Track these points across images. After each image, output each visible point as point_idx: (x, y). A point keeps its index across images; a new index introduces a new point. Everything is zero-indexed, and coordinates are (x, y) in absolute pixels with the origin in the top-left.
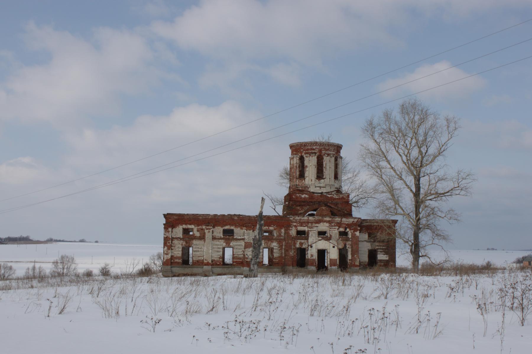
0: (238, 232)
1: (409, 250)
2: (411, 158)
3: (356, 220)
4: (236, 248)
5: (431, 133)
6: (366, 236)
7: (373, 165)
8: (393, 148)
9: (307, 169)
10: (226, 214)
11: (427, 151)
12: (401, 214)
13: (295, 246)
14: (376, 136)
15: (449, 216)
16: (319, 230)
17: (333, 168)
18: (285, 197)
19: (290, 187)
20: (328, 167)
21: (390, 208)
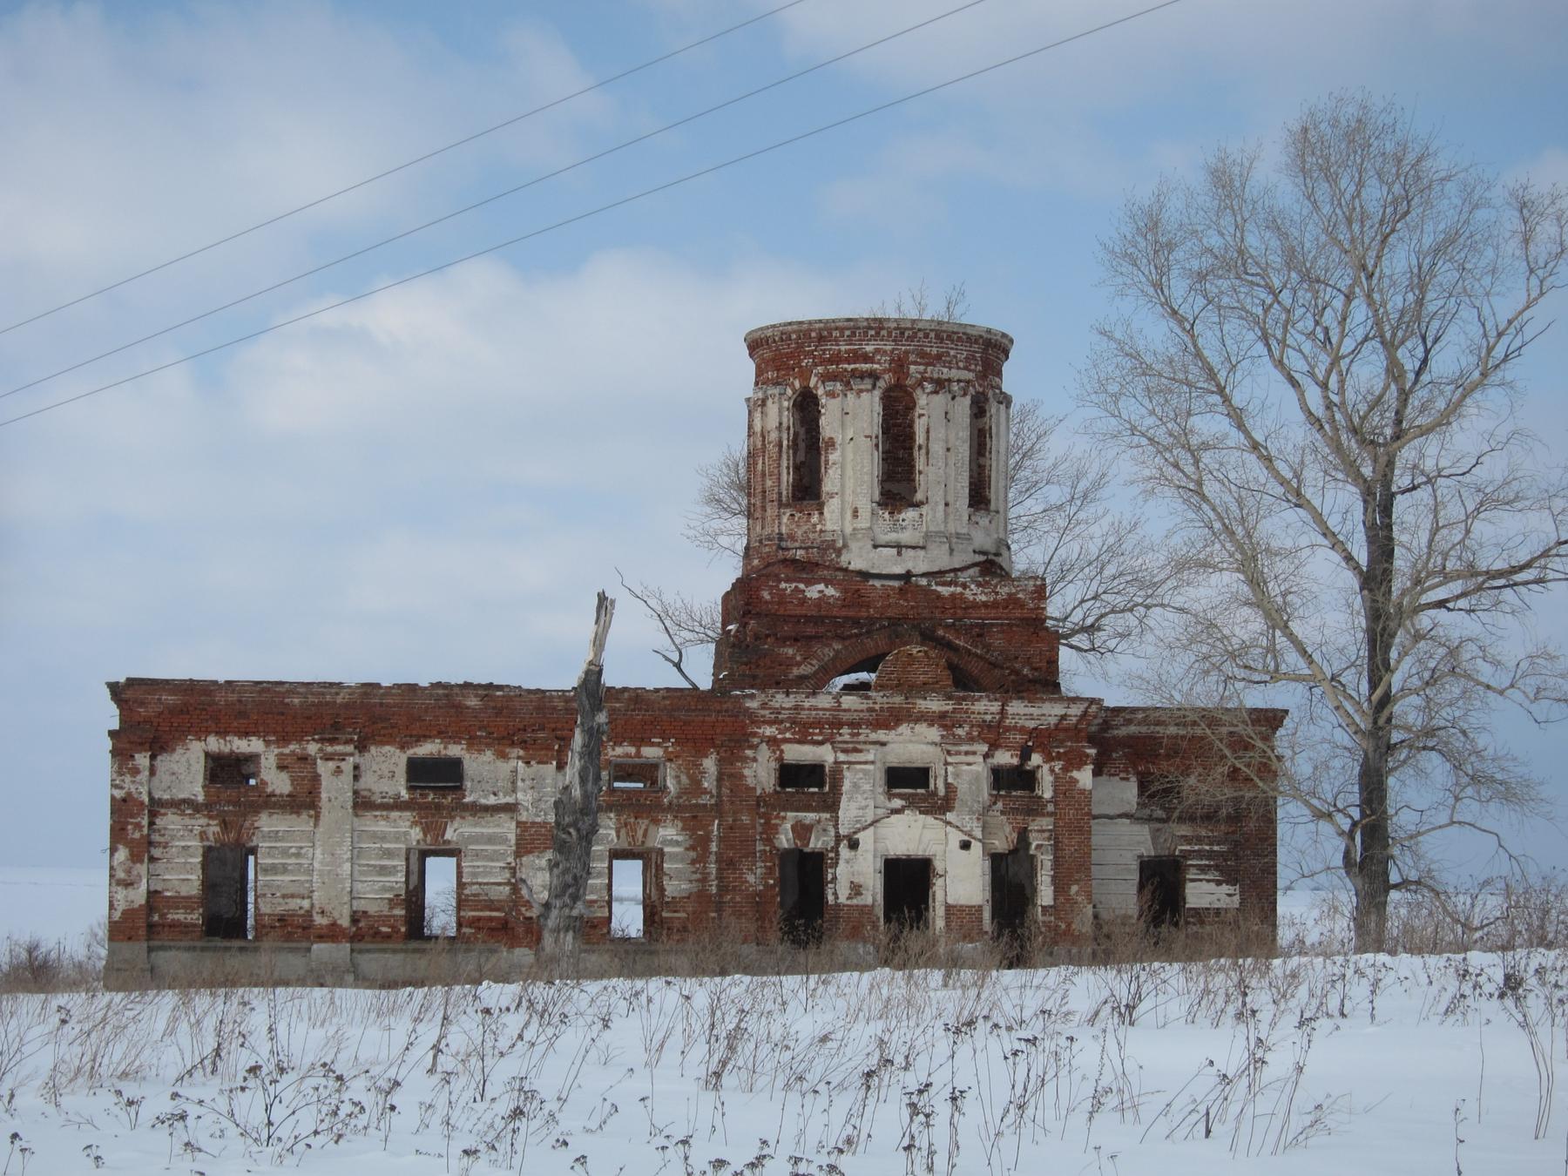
0: (485, 770)
1: (1338, 860)
2: (1350, 395)
3: (1076, 710)
4: (477, 855)
5: (1446, 274)
6: (1125, 793)
7: (1161, 434)
8: (1260, 348)
9: (834, 457)
10: (424, 683)
11: (1425, 362)
12: (1299, 679)
13: (769, 841)
14: (1178, 287)
15: (1530, 684)
16: (894, 761)
17: (964, 451)
18: (727, 598)
19: (747, 548)
20: (937, 448)
21: (1245, 647)
